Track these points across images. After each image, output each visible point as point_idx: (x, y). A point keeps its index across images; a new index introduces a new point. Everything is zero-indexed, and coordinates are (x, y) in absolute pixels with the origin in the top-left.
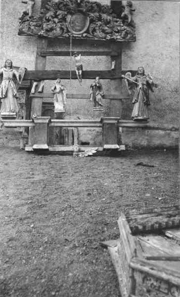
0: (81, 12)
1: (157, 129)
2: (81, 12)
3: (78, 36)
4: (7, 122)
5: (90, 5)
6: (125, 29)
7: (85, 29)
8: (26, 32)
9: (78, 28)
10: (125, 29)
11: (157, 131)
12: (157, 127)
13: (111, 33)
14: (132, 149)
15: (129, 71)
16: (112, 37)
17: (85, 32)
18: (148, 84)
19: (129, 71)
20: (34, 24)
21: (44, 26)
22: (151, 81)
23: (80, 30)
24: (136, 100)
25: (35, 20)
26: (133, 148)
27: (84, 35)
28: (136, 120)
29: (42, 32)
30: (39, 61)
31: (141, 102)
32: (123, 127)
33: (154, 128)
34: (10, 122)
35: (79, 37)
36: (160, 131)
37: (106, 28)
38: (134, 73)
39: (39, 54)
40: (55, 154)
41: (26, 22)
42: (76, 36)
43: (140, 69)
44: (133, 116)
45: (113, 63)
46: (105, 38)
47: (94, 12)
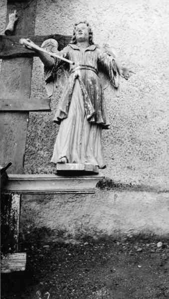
1: (139, 188)
11: (138, 195)
12: (138, 183)
14: (74, 242)
15: (51, 37)
18: (102, 68)
19: (51, 37)
22: (107, 62)
24: (62, 112)
26: (77, 239)
28: (60, 173)
31: (79, 118)
32: (23, 194)
33: (130, 187)
34: (14, 177)
36: (145, 193)
38: (62, 41)
40: (125, 189)
43: (80, 26)
44: (54, 159)
45: (12, 16)
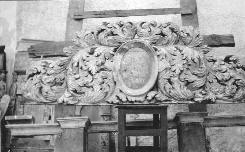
0: (141, 45)
2: (141, 45)
3: (138, 99)
4: (17, 129)
5: (158, 31)
6: (231, 77)
7: (151, 84)
8: (34, 97)
9: (138, 81)
10: (231, 77)
13: (204, 87)
16: (207, 98)
17: (152, 90)
20: (51, 79)
21: (70, 82)
23: (141, 86)
25: (52, 71)
27: (151, 95)
29: (65, 97)
30: (71, 27)
34: (21, 128)
35: (140, 102)
37: (193, 78)
39: (72, 16)
41: (35, 77)
42: (133, 99)
46: (192, 100)
47: (167, 44)
